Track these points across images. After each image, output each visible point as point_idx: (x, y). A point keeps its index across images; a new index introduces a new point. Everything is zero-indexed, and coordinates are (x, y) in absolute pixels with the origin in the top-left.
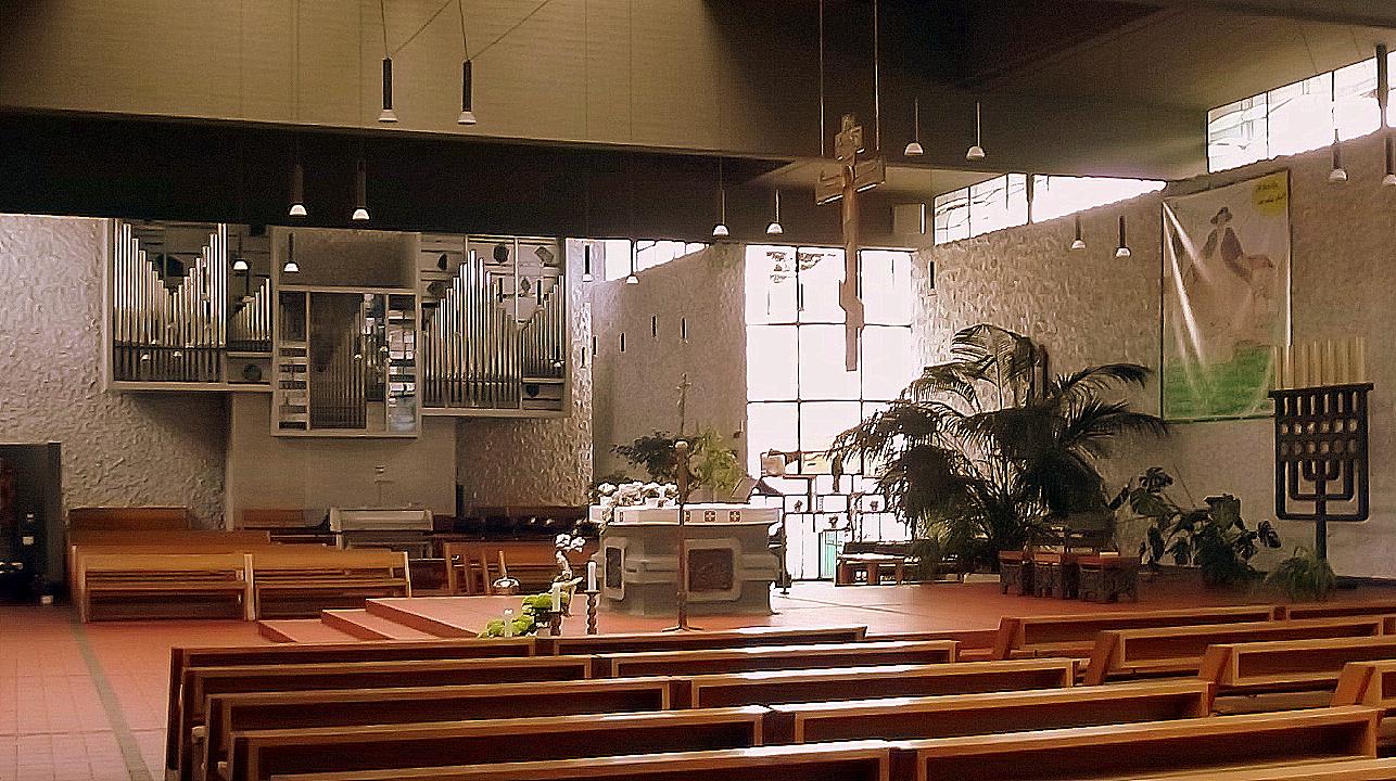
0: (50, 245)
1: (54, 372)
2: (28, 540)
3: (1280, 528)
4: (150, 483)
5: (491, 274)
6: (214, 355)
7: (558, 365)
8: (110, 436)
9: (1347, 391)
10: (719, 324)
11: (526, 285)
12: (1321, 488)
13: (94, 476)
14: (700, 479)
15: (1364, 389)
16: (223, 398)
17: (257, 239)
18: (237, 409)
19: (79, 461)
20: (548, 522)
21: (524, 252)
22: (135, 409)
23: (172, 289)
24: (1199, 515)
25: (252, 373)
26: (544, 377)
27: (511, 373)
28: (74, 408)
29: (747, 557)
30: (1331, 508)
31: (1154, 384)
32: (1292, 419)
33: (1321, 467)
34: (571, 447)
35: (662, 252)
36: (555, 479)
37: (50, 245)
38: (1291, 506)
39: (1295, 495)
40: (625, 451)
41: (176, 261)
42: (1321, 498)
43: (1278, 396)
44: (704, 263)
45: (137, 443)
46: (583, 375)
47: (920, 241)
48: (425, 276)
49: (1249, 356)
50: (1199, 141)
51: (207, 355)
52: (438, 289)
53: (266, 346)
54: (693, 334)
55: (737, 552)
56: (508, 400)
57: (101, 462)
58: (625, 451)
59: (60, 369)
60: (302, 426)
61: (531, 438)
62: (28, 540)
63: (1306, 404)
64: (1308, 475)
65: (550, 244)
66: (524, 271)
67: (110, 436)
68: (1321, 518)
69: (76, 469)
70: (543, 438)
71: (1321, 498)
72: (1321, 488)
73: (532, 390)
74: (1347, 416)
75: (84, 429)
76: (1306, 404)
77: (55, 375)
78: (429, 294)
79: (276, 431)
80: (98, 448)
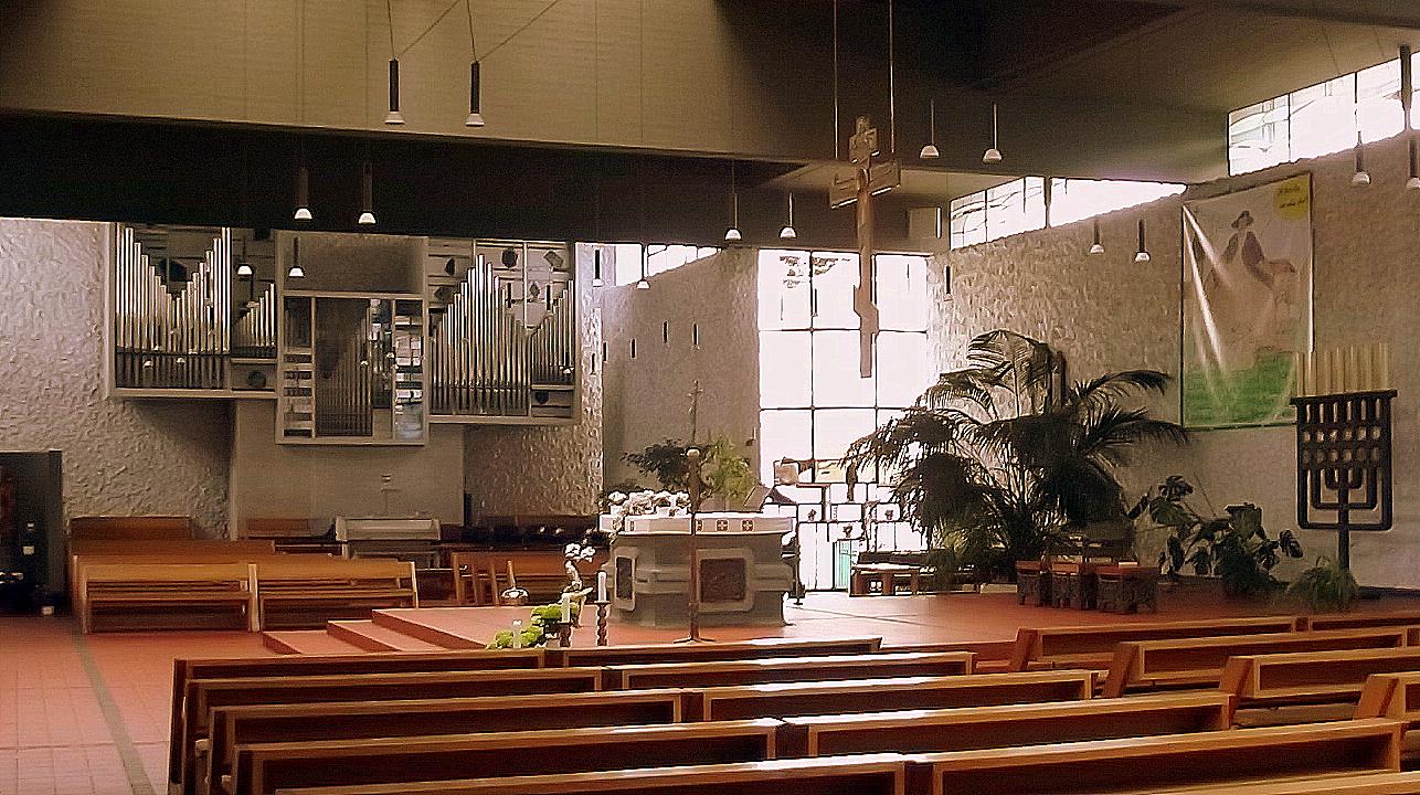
0: (51, 249)
1: (55, 379)
2: (28, 550)
3: (1302, 537)
4: (152, 491)
5: (500, 279)
6: (218, 361)
7: (568, 371)
8: (112, 443)
9: (1370, 398)
10: (731, 330)
11: (535, 290)
12: (1343, 497)
13: (96, 485)
14: (712, 488)
15: (1387, 396)
16: (227, 406)
17: (262, 244)
18: (241, 416)
19: (81, 469)
20: (558, 531)
21: (533, 256)
22: (137, 416)
23: (175, 294)
24: (1219, 525)
25: (257, 380)
26: (553, 384)
27: (519, 380)
28: (75, 415)
29: (760, 567)
30: (1354, 517)
31: (1173, 391)
32: (1314, 427)
33: (1344, 476)
34: (581, 455)
35: (673, 257)
36: (564, 487)
37: (51, 249)
38: (1314, 515)
39: (1317, 504)
40: (635, 459)
41: (179, 265)
42: (1343, 507)
43: (1300, 403)
44: (716, 268)
45: (140, 450)
46: (593, 382)
47: (936, 245)
48: (433, 281)
49: (1271, 363)
50: (1220, 143)
51: (211, 361)
52: (446, 294)
53: (271, 352)
54: (705, 339)
55: (749, 562)
56: (517, 407)
57: (103, 471)
58: (635, 459)
59: (61, 376)
60: (307, 434)
61: (540, 446)
62: (28, 550)
63: (1328, 412)
64: (1330, 483)
65: (559, 249)
66: (533, 276)
67: (112, 443)
68: (1344, 528)
69: (77, 477)
70: (553, 446)
71: (1343, 507)
72: (1343, 497)
73: (542, 397)
74: (1370, 424)
75: (86, 437)
76: (1328, 412)
77: (56, 381)
78: (436, 300)
79: (281, 439)
80: (100, 456)
